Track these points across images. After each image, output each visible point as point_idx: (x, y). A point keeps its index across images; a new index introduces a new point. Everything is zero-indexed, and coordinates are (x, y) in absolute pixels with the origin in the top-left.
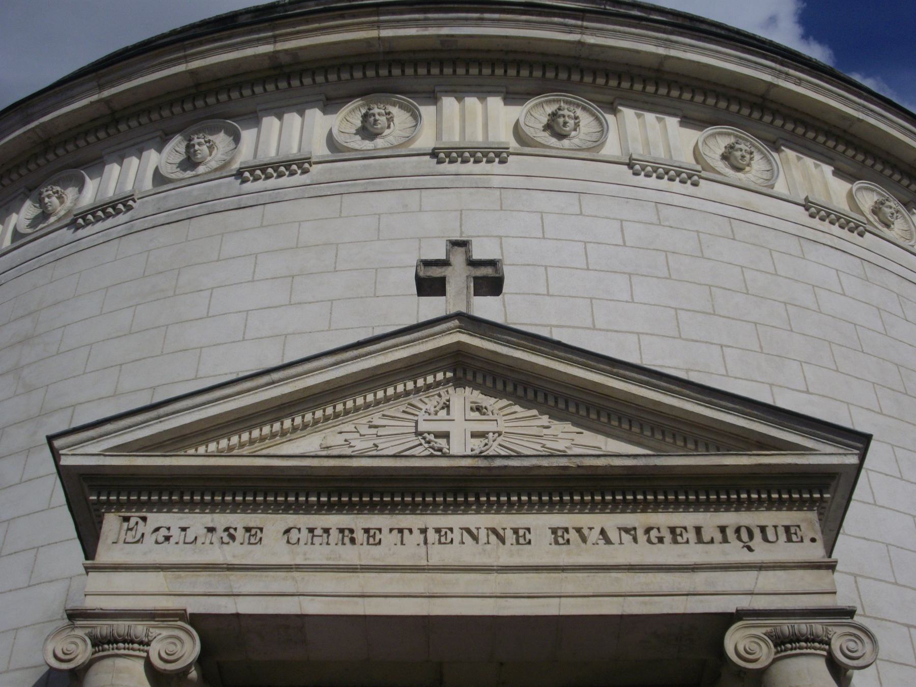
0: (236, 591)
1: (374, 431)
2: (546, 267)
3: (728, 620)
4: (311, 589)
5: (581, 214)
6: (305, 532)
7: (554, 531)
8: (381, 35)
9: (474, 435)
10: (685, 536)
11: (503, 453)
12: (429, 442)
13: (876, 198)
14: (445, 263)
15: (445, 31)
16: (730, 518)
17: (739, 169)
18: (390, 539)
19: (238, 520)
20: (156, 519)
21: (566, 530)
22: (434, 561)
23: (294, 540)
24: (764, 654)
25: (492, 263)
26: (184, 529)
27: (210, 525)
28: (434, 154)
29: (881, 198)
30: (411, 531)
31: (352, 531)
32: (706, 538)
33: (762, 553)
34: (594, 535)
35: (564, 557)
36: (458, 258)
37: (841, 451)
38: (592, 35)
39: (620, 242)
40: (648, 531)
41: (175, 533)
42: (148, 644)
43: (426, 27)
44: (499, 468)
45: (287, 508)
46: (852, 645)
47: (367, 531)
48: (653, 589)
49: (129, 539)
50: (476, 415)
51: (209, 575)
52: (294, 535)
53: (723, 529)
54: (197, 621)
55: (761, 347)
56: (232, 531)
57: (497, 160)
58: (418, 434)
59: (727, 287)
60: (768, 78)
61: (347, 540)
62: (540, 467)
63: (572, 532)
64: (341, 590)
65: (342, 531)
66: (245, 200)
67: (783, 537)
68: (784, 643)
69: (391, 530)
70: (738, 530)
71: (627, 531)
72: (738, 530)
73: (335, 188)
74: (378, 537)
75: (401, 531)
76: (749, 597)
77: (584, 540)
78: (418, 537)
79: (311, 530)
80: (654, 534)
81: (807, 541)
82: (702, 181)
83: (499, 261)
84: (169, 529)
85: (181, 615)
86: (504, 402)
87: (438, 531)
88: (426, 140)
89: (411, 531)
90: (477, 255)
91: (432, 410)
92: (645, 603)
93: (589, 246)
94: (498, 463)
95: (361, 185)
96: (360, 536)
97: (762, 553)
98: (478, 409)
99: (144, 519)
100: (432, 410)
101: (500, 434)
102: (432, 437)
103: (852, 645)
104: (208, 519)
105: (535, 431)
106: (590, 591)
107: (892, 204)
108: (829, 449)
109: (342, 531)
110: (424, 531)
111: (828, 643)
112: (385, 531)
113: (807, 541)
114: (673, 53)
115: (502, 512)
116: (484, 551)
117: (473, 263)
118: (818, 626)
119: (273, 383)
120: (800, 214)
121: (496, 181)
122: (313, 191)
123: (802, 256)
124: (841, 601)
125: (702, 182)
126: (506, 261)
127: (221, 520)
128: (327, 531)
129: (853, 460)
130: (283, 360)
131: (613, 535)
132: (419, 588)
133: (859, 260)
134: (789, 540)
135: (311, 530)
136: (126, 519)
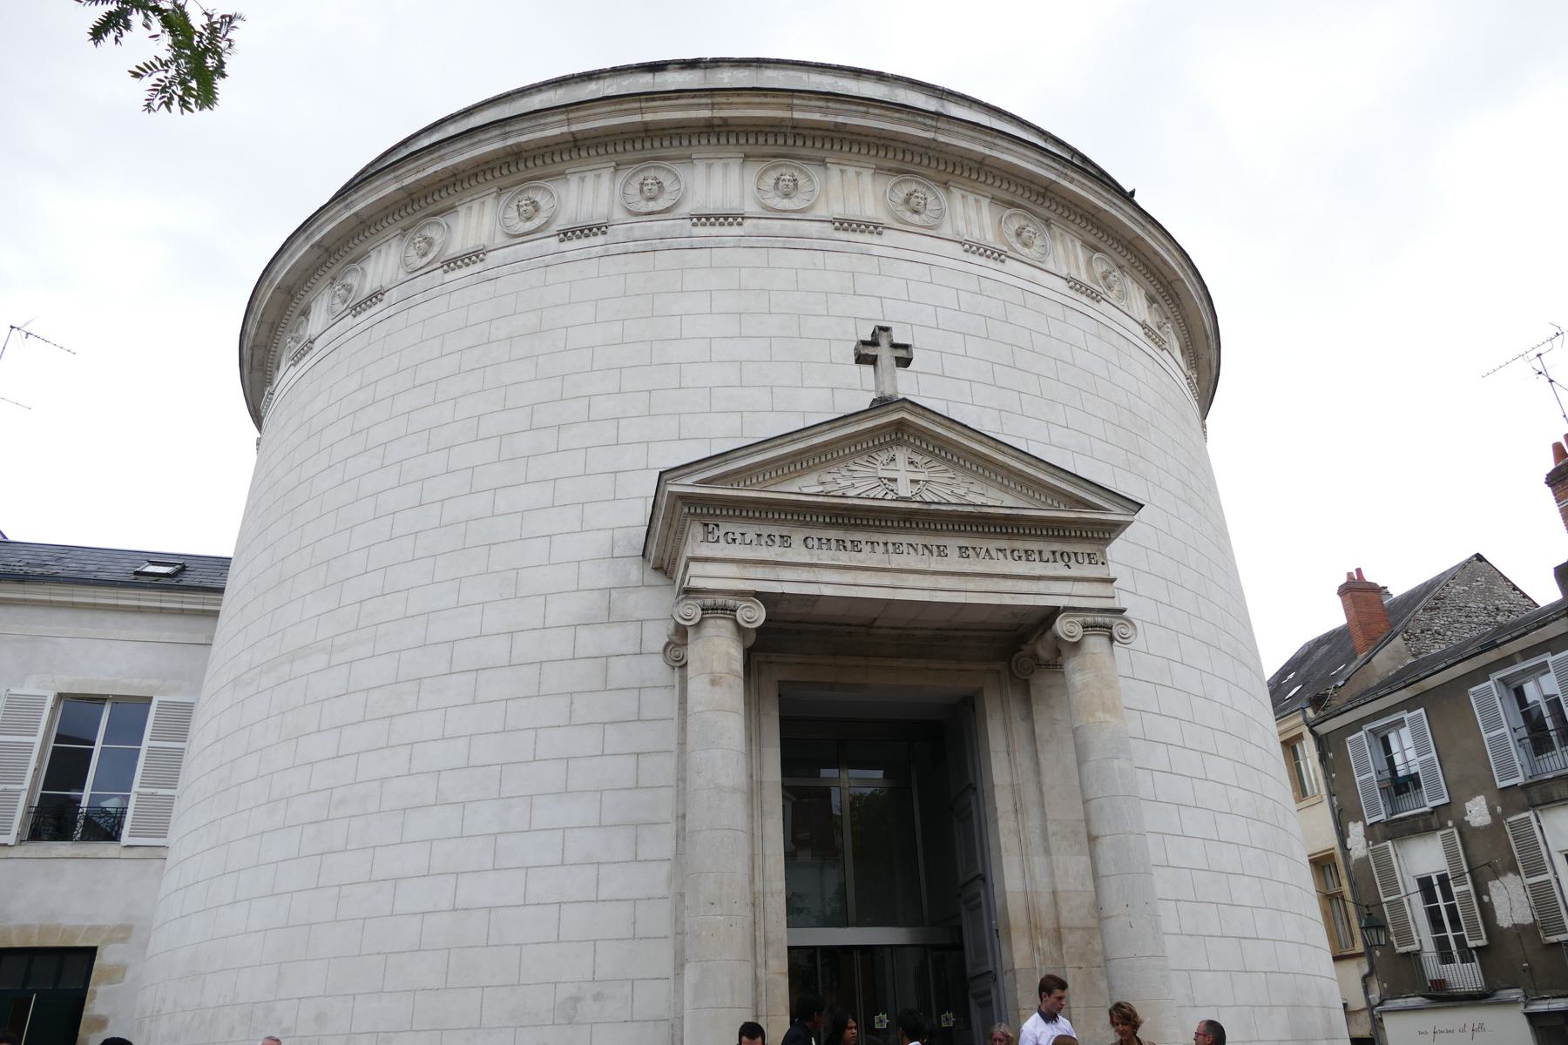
0: (781, 578)
1: (850, 473)
2: (912, 325)
3: (1055, 612)
4: (825, 579)
5: (932, 282)
6: (816, 541)
7: (960, 548)
8: (794, 116)
10: (1033, 556)
11: (936, 501)
12: (885, 485)
13: (1105, 268)
15: (840, 119)
16: (1057, 547)
17: (1025, 245)
18: (866, 548)
19: (775, 531)
20: (725, 527)
21: (967, 548)
22: (894, 566)
23: (810, 546)
24: (1078, 631)
25: (906, 347)
26: (743, 534)
27: (759, 533)
29: (1109, 270)
30: (878, 543)
31: (843, 541)
32: (1045, 559)
33: (1075, 571)
34: (983, 551)
35: (966, 566)
37: (1126, 513)
38: (942, 134)
39: (957, 308)
40: (1013, 551)
41: (738, 536)
42: (735, 611)
43: (826, 114)
44: (934, 510)
45: (806, 524)
47: (852, 542)
48: (1014, 590)
49: (710, 540)
50: (912, 468)
52: (809, 541)
53: (1054, 553)
55: (1042, 394)
56: (772, 537)
57: (875, 232)
59: (1022, 346)
60: (1053, 177)
61: (841, 547)
62: (957, 511)
63: (971, 550)
65: (838, 541)
66: (696, 242)
67: (1087, 561)
68: (1087, 627)
69: (867, 542)
70: (1062, 554)
71: (1000, 550)
72: (1062, 554)
73: (762, 241)
74: (860, 546)
75: (872, 543)
76: (1068, 597)
77: (978, 555)
78: (881, 549)
79: (820, 540)
80: (1016, 553)
81: (1100, 564)
82: (1008, 259)
83: (911, 345)
84: (733, 533)
85: (757, 595)
86: (927, 459)
87: (894, 544)
89: (878, 543)
90: (896, 341)
91: (885, 462)
92: (1013, 598)
93: (938, 308)
94: (934, 507)
95: (779, 242)
96: (848, 545)
97: (1075, 571)
99: (717, 526)
100: (885, 462)
104: (757, 529)
105: (946, 481)
106: (983, 589)
107: (1116, 274)
108: (1118, 511)
109: (838, 541)
110: (886, 544)
111: (1111, 628)
112: (863, 543)
113: (1100, 564)
114: (995, 154)
116: (922, 559)
117: (895, 346)
118: (1106, 620)
119: (794, 440)
120: (1061, 285)
121: (876, 250)
122: (746, 242)
123: (1062, 319)
124: (1115, 604)
125: (1008, 260)
126: (917, 344)
127: (766, 530)
128: (829, 540)
129: (1422, 829)
131: (994, 553)
132: (887, 582)
133: (1096, 322)
134: (1090, 563)
135: (820, 540)
136: (707, 525)
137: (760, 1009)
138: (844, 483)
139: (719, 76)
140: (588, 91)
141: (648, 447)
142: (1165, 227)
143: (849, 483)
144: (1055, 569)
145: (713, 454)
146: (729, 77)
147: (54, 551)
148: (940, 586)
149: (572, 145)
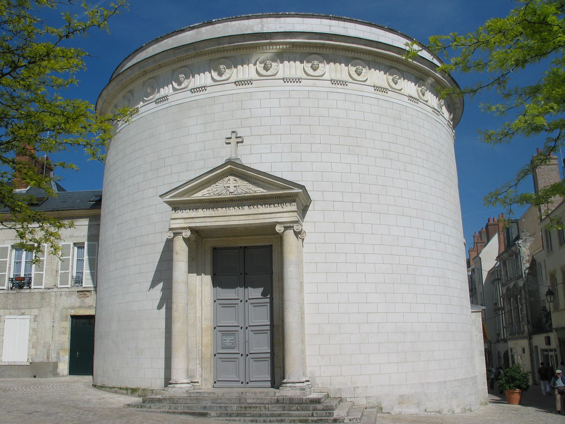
9: (235, 187)
14: (230, 138)
22: (228, 214)
28: (235, 83)
36: (234, 136)
46: (297, 227)
48: (264, 218)
50: (235, 182)
51: (246, 193)
54: (190, 228)
58: (224, 187)
64: (223, 220)
88: (233, 79)
98: (235, 180)
101: (239, 186)
102: (227, 188)
103: (297, 227)
115: (25, 287)
130: (262, 28)
132: (225, 220)
137: (524, 329)
138: (214, 190)
139: (202, 30)
140: (164, 43)
141: (213, 155)
142: (383, 42)
143: (216, 189)
144: (278, 209)
145: (196, 177)
146: (205, 30)
147: (85, 194)
148: (241, 219)
149: (159, 66)
